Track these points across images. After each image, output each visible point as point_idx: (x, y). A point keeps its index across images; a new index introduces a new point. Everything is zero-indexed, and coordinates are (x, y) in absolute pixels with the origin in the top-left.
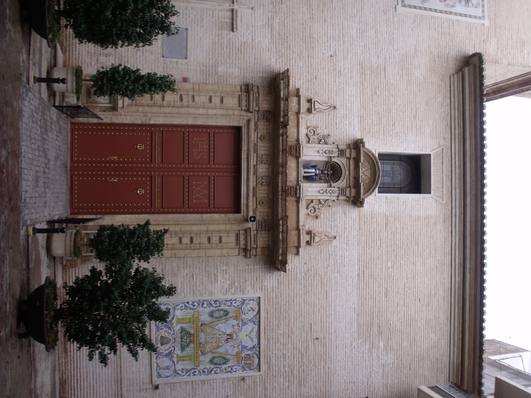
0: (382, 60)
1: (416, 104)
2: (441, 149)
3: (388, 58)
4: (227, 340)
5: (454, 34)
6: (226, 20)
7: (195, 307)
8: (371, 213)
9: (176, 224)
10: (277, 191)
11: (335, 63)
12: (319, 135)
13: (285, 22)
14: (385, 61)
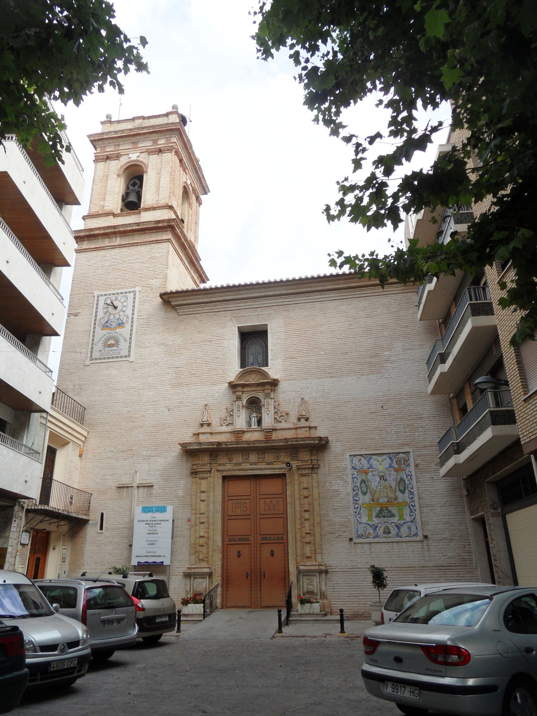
2: (232, 318)
4: (385, 480)
6: (145, 492)
7: (359, 507)
9: (295, 523)
10: (268, 446)
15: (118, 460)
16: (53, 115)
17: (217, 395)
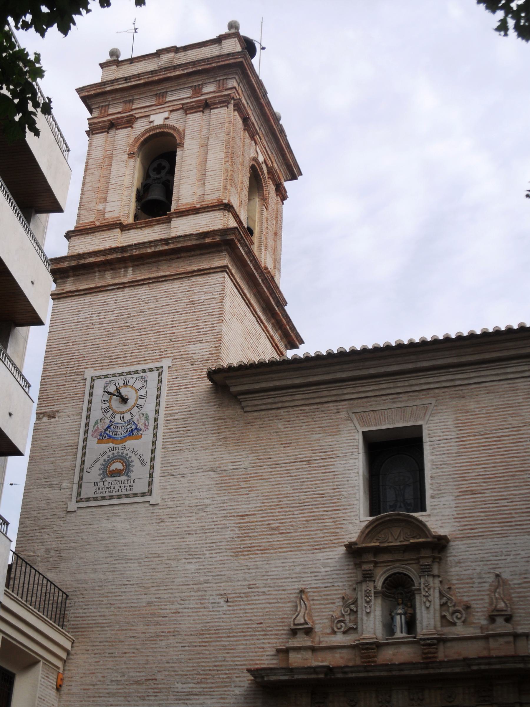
0: (228, 522)
1: (290, 463)
3: (225, 512)
5: (185, 411)
8: (457, 520)
11: (237, 595)
12: (344, 613)
13: (181, 675)
14: (230, 516)
15: (129, 699)
16: (22, 55)
17: (323, 570)
